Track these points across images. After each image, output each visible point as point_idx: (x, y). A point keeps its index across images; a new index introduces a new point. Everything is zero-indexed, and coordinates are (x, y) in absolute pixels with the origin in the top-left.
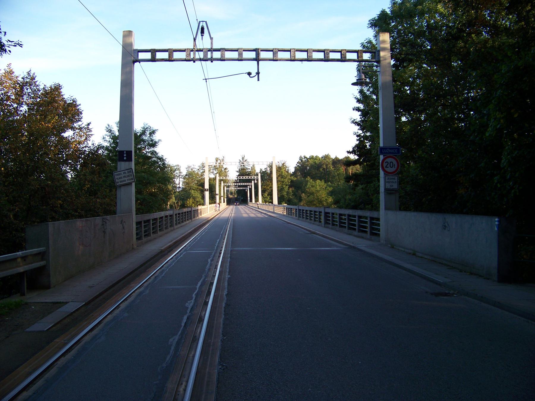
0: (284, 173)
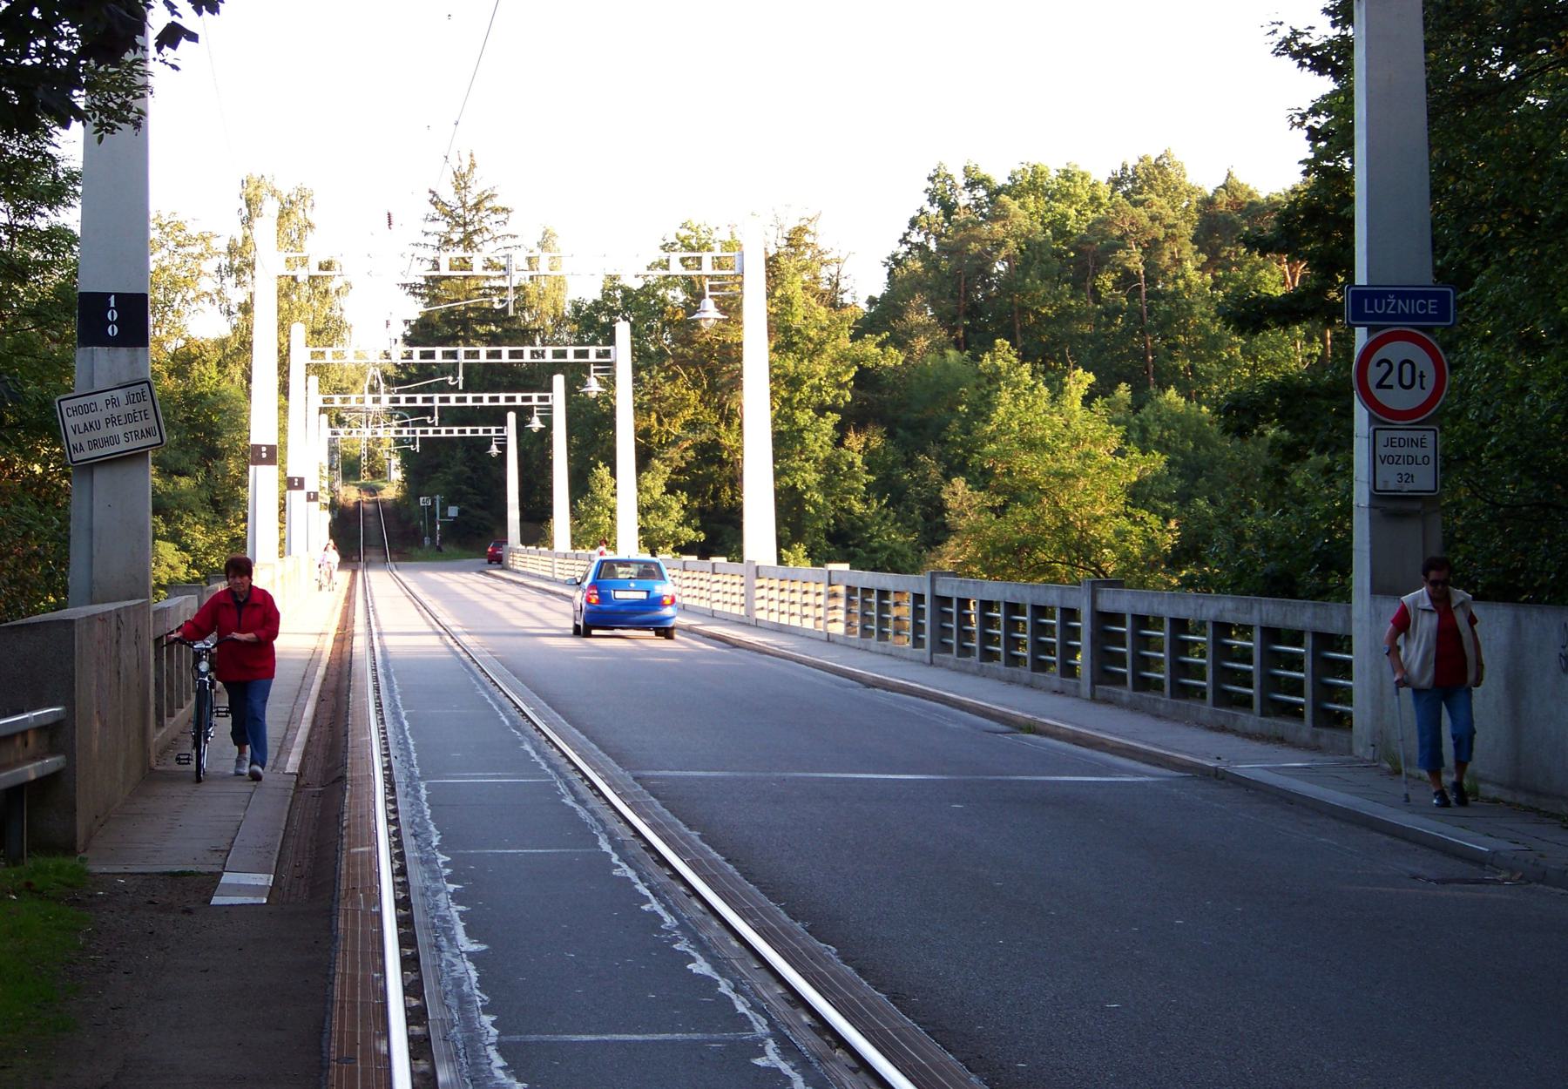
0: (801, 312)
